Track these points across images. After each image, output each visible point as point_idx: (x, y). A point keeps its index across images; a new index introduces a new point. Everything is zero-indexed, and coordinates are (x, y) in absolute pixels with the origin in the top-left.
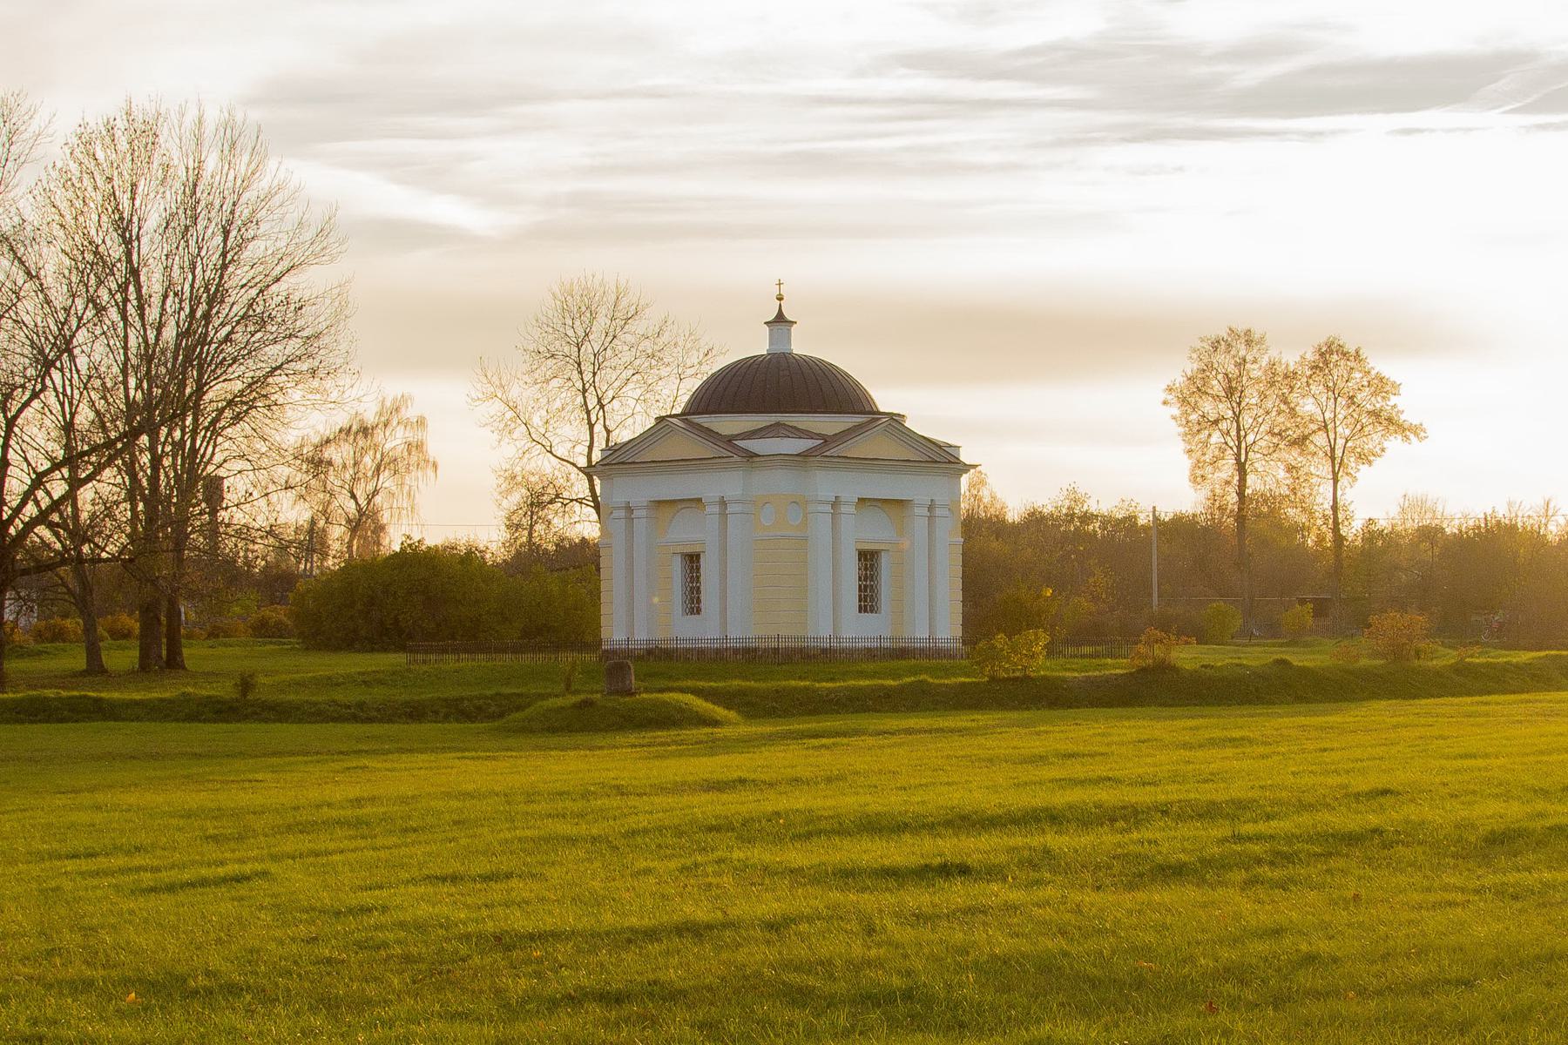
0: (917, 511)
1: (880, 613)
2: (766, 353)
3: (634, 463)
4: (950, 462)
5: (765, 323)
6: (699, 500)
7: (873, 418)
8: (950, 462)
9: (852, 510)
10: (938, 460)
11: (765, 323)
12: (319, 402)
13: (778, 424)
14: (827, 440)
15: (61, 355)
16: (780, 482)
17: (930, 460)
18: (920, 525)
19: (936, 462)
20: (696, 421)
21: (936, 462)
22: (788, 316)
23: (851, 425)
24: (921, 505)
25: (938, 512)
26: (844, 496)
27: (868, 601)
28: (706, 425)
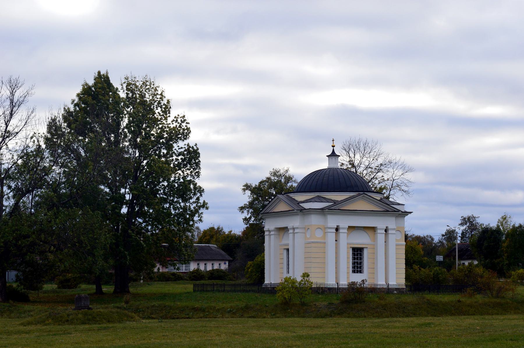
0: (379, 231)
1: (364, 273)
2: (327, 168)
3: (271, 213)
4: (395, 211)
5: (327, 156)
6: (287, 228)
7: (359, 194)
8: (395, 211)
9: (346, 231)
10: (390, 211)
11: (327, 156)
12: (56, 170)
13: (319, 197)
14: (335, 202)
15: (465, 221)
16: (315, 220)
17: (386, 210)
18: (381, 237)
19: (389, 211)
20: (291, 196)
21: (389, 211)
22: (337, 153)
23: (349, 196)
24: (381, 229)
25: (390, 232)
26: (341, 225)
27: (357, 268)
28: (293, 197)
